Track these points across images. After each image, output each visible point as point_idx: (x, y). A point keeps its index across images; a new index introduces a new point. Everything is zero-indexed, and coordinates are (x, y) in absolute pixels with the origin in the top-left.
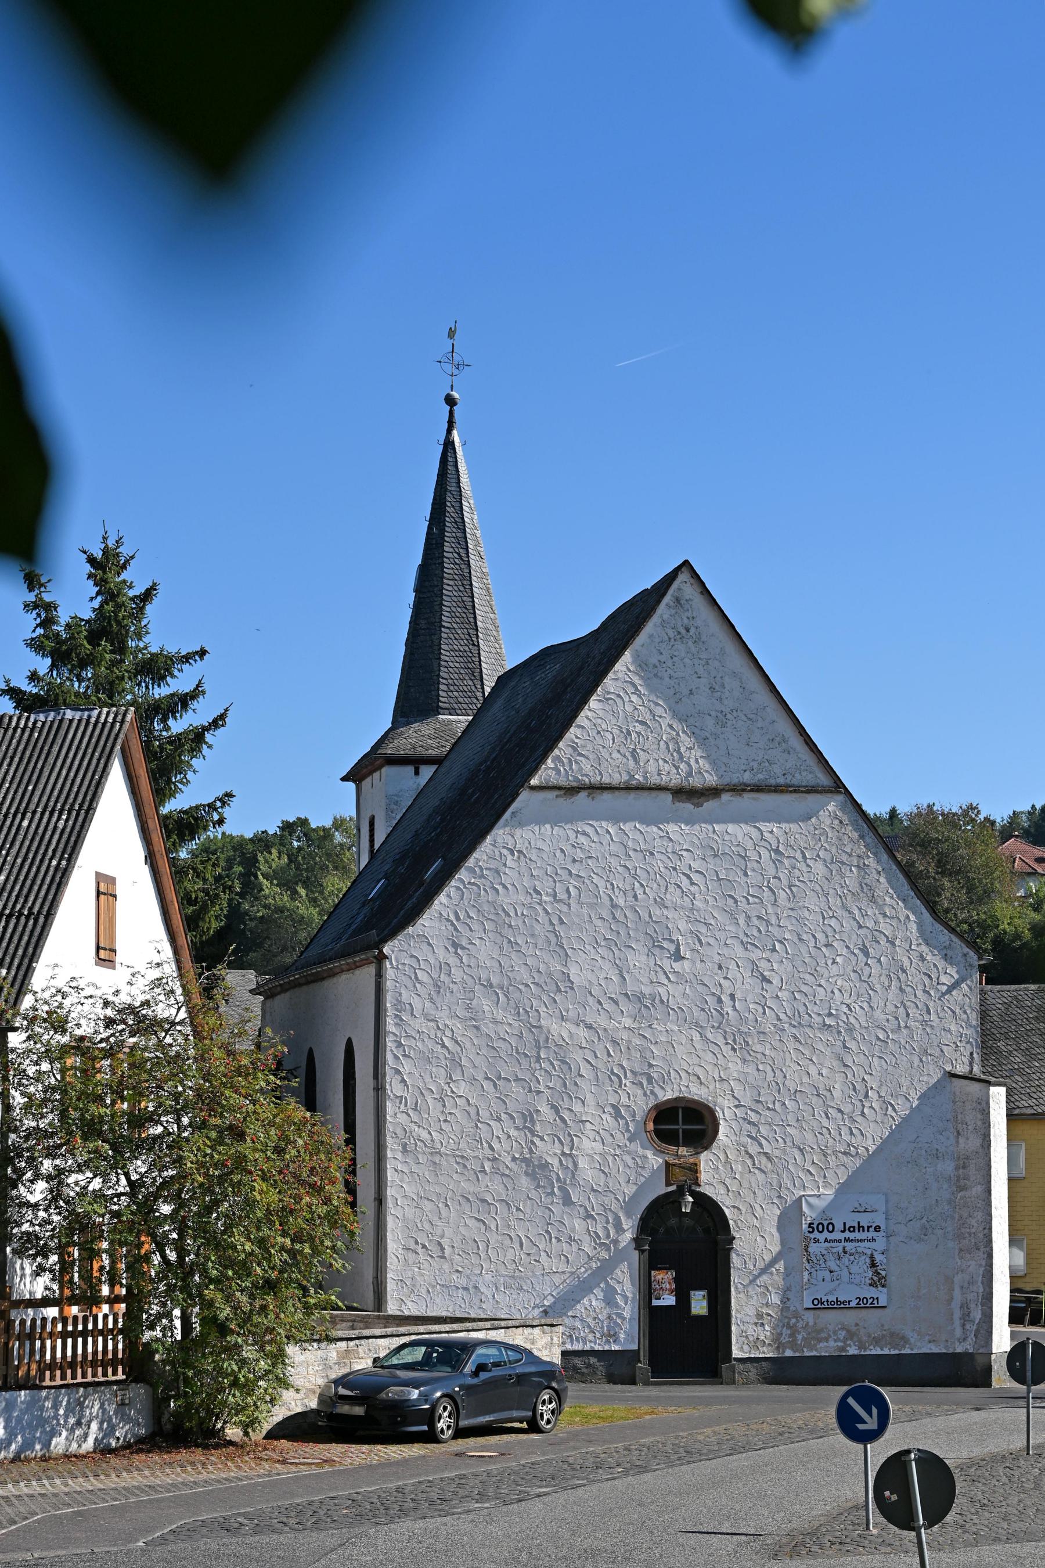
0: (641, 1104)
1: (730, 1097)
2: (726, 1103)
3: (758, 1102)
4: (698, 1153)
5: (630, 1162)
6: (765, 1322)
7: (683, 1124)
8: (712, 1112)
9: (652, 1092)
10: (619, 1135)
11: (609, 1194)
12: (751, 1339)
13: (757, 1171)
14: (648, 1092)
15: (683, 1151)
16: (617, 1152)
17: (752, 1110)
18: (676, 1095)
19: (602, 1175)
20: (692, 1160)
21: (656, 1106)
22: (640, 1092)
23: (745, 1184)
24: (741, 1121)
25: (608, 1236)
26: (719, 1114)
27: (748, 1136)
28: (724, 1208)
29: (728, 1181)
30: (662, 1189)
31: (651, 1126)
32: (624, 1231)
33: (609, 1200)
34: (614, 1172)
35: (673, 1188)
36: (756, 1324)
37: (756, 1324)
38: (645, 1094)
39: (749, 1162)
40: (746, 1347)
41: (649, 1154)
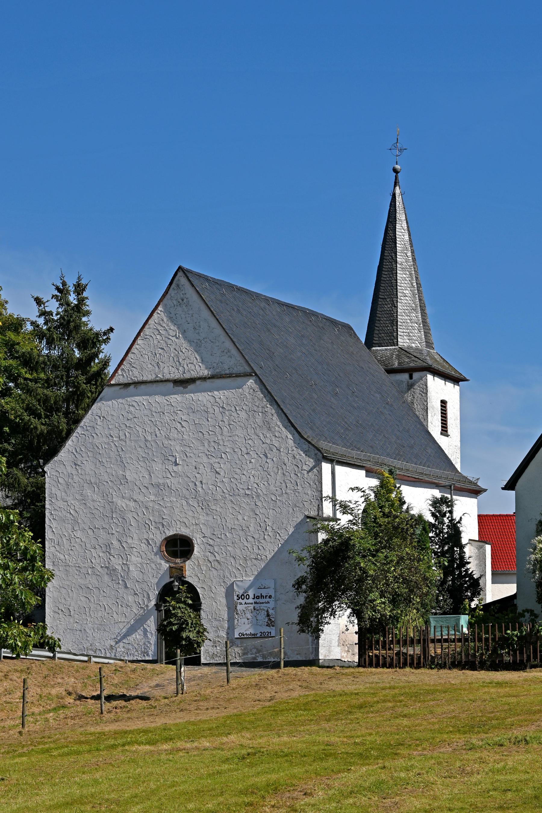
0: (159, 538)
1: (200, 533)
2: (198, 536)
3: (214, 534)
4: (185, 561)
5: (154, 567)
6: (217, 645)
7: (179, 547)
8: (191, 540)
9: (164, 532)
10: (149, 554)
11: (144, 583)
12: (211, 654)
13: (213, 569)
14: (162, 532)
15: (178, 560)
16: (148, 562)
17: (211, 539)
18: (175, 532)
19: (141, 574)
20: (181, 565)
21: (166, 539)
22: (158, 532)
23: (207, 576)
24: (205, 544)
25: (144, 604)
26: (195, 542)
27: (209, 552)
28: (197, 589)
29: (199, 575)
30: (168, 580)
31: (164, 548)
32: (151, 601)
33: (144, 586)
34: (146, 572)
35: (172, 579)
36: (213, 646)
37: (213, 646)
38: (161, 533)
39: (209, 565)
40: (208, 658)
41: (163, 562)
